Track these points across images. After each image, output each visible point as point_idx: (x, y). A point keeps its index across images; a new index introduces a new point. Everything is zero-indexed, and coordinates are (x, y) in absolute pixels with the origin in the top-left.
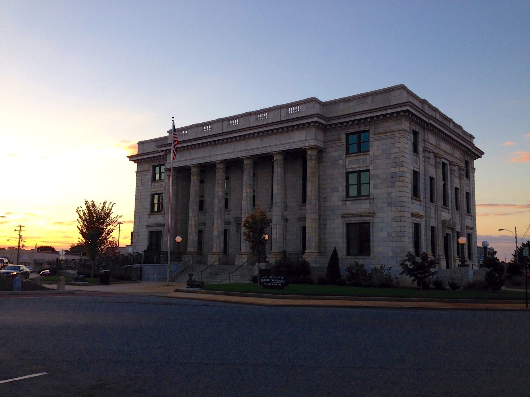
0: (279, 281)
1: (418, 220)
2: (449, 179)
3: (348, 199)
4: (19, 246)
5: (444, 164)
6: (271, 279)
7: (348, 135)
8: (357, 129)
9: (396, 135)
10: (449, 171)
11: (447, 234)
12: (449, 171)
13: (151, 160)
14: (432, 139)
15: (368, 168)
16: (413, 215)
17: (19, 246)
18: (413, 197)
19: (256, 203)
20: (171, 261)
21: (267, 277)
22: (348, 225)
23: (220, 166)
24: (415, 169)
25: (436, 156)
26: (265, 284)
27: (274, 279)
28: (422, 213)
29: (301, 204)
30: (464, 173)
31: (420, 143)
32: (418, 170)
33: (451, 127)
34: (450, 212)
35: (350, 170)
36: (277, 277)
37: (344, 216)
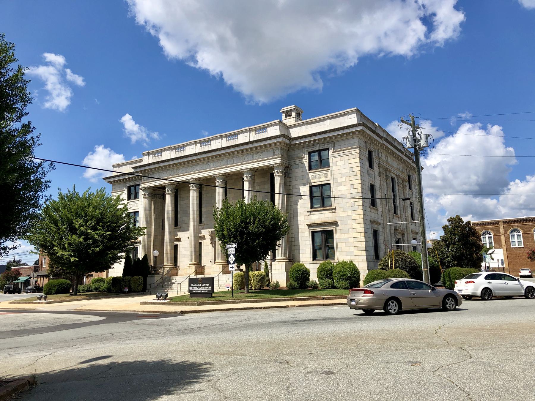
0: (206, 288)
1: (376, 227)
2: (397, 191)
3: (313, 210)
4: (415, 141)
5: (393, 179)
7: (310, 154)
8: (317, 148)
10: (397, 184)
11: (399, 239)
12: (397, 184)
13: (132, 180)
14: (383, 155)
15: (329, 182)
16: (310, 226)
17: (415, 141)
19: (203, 220)
21: (196, 285)
22: (313, 233)
24: (371, 182)
26: (194, 291)
28: (380, 221)
29: (309, 210)
30: (407, 184)
32: (373, 183)
33: (396, 145)
35: (313, 184)
36: (204, 285)
37: (310, 226)
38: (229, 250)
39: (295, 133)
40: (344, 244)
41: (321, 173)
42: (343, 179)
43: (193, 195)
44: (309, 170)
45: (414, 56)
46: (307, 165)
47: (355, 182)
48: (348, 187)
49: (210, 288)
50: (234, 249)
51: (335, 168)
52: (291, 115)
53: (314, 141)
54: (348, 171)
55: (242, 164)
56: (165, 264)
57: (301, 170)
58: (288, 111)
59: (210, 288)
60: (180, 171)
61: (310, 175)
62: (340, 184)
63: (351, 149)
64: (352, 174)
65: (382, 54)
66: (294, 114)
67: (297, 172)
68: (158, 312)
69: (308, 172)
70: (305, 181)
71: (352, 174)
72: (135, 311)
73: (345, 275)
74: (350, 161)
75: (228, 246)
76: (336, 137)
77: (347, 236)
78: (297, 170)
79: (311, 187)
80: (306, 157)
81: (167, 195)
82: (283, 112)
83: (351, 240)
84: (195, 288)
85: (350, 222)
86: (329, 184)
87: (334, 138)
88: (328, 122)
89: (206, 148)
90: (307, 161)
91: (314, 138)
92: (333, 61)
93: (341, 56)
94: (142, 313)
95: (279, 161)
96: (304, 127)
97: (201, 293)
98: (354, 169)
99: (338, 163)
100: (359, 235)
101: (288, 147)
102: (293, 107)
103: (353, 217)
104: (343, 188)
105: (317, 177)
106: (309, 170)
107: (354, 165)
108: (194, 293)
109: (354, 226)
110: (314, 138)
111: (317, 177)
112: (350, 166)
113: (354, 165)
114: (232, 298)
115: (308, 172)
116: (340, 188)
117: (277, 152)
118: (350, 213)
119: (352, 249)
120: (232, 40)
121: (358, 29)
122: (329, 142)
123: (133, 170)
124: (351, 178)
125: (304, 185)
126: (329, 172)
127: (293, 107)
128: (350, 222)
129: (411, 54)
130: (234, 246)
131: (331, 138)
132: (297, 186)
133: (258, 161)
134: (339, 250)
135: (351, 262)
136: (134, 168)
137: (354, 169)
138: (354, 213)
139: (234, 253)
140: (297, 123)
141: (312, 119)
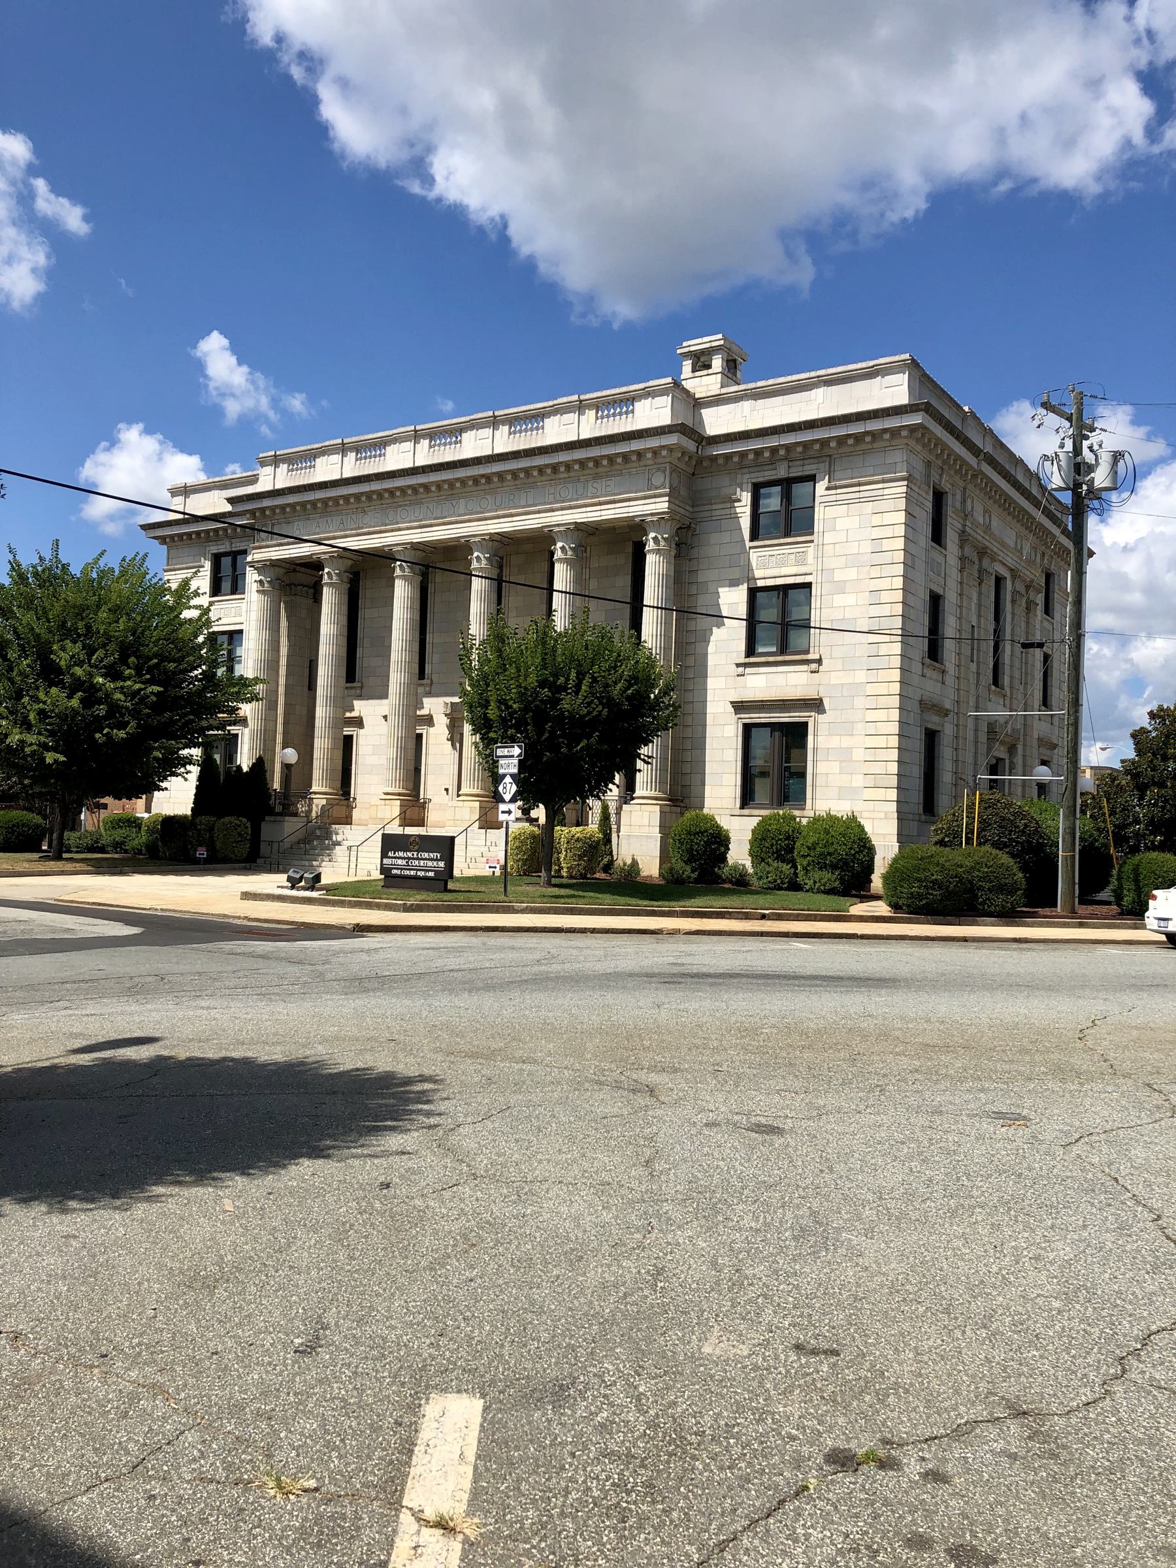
0: (430, 863)
1: (934, 721)
3: (752, 660)
5: (999, 580)
6: (409, 858)
8: (782, 472)
9: (714, 513)
12: (1009, 597)
15: (807, 579)
18: (928, 661)
20: (991, 780)
21: (401, 854)
22: (748, 729)
23: (479, 561)
25: (983, 552)
26: (394, 872)
27: (417, 859)
29: (743, 660)
31: (949, 520)
33: (1020, 478)
34: (1008, 702)
35: (760, 583)
37: (740, 707)
38: (502, 762)
39: (716, 422)
40: (835, 767)
41: (786, 550)
42: (852, 574)
43: (402, 593)
44: (752, 540)
45: (1104, 196)
46: (745, 523)
47: (885, 584)
48: (865, 598)
49: (442, 864)
50: (516, 761)
51: (829, 538)
52: (709, 367)
53: (774, 450)
54: (867, 547)
55: (553, 510)
56: (314, 788)
57: (726, 537)
58: (703, 352)
59: (442, 864)
60: (367, 519)
61: (754, 556)
62: (840, 588)
63: (884, 481)
64: (878, 559)
65: (1004, 187)
66: (717, 363)
67: (715, 544)
68: (292, 923)
69: (748, 544)
70: (736, 573)
71: (878, 559)
72: (225, 916)
73: (830, 854)
74: (877, 520)
75: (500, 752)
76: (841, 440)
77: (846, 742)
78: (714, 538)
79: (753, 593)
80: (746, 497)
81: (325, 589)
82: (686, 355)
83: (859, 754)
84: (400, 862)
85: (860, 702)
86: (808, 586)
87: (833, 444)
88: (819, 393)
89: (448, 454)
90: (748, 510)
91: (773, 442)
92: (847, 199)
93: (874, 185)
94: (239, 922)
95: (661, 505)
96: (747, 405)
97: (416, 878)
98: (886, 544)
99: (840, 524)
100: (881, 742)
101: (695, 464)
102: (716, 339)
103: (870, 690)
104: (849, 599)
105: (773, 564)
106: (752, 540)
107: (888, 532)
108: (396, 876)
109: (872, 715)
110: (773, 442)
111: (773, 564)
112: (877, 533)
113: (888, 532)
114: (502, 897)
115: (748, 544)
116: (839, 600)
117: (658, 479)
118: (861, 676)
119: (858, 781)
120: (545, 119)
121: (938, 101)
122: (818, 458)
123: (228, 508)
124: (875, 572)
125: (734, 583)
126: (811, 550)
127: (716, 339)
128: (860, 702)
129: (1095, 189)
130: (516, 751)
131: (824, 443)
132: (711, 589)
133: (600, 504)
134: (820, 781)
135: (853, 819)
136: (231, 500)
137: (886, 544)
138: (872, 676)
139: (515, 771)
140: (724, 390)
141: (771, 382)
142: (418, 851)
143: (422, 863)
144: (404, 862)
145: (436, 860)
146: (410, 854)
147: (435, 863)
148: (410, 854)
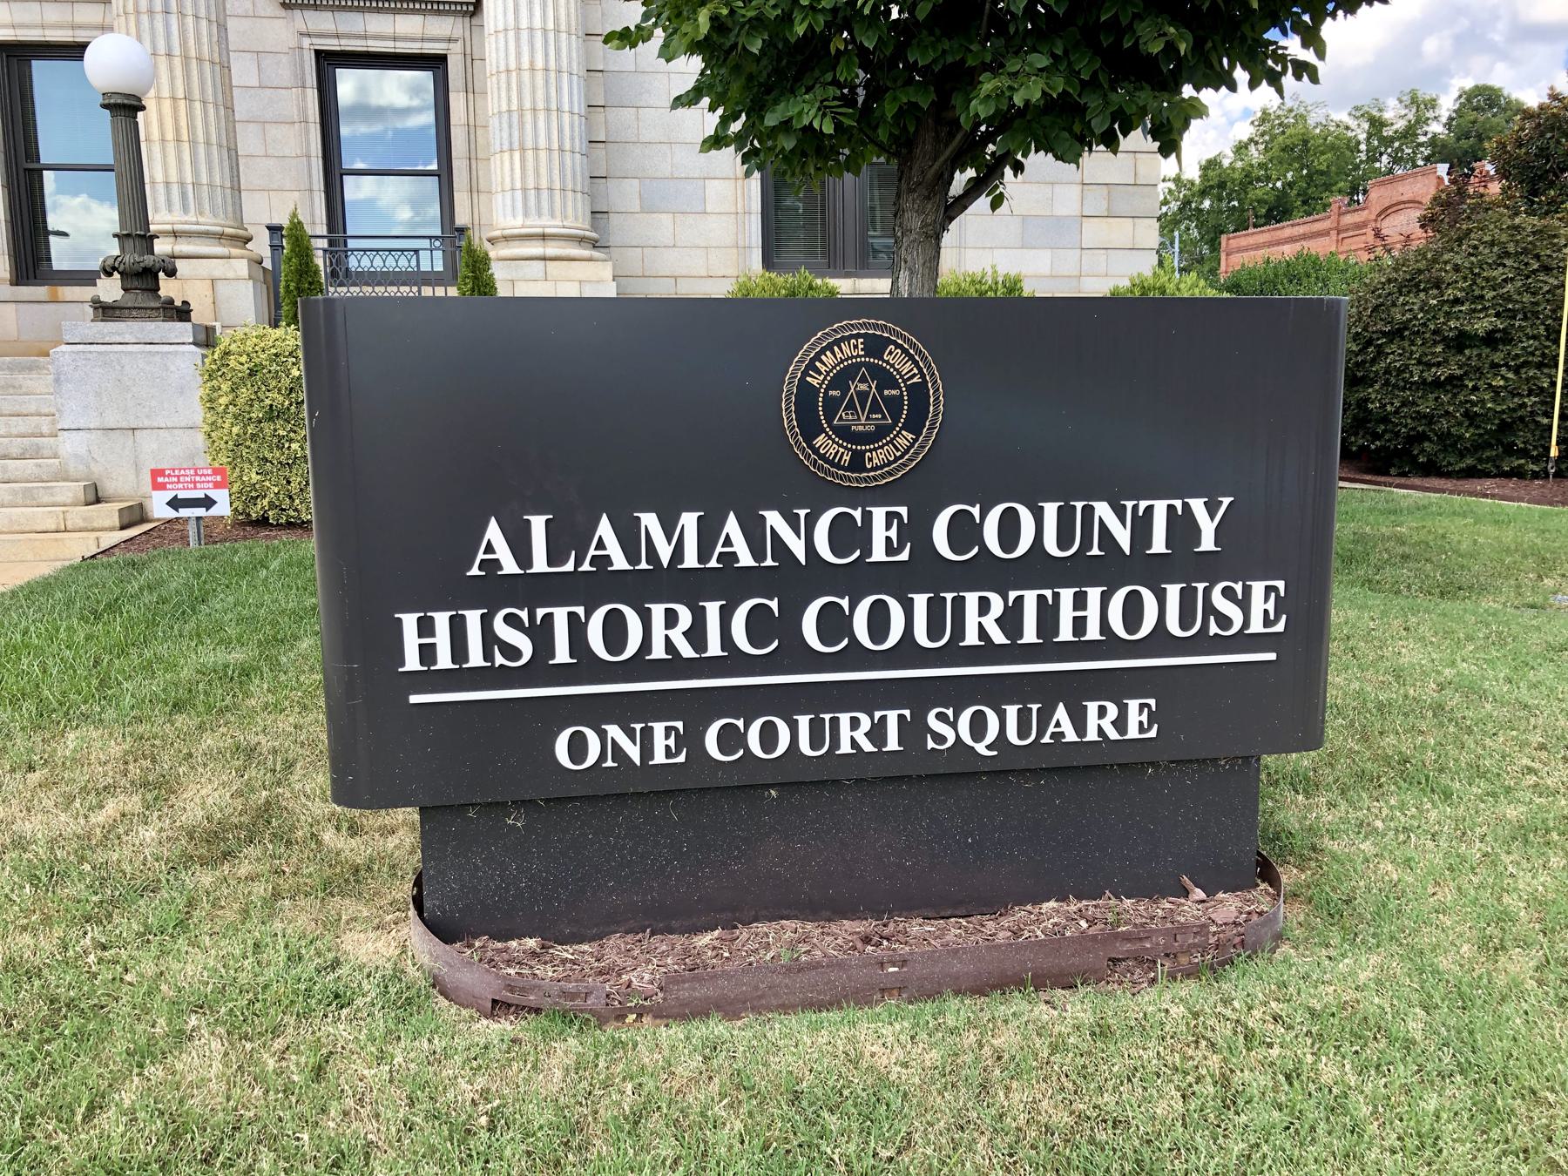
0: (1094, 611)
6: (794, 580)
21: (674, 538)
27: (920, 572)
36: (1041, 527)
84: (661, 630)
97: (922, 777)
108: (623, 789)
142: (918, 493)
143: (980, 618)
144: (731, 626)
145: (1183, 562)
146: (805, 537)
147: (1163, 608)
148: (805, 537)
